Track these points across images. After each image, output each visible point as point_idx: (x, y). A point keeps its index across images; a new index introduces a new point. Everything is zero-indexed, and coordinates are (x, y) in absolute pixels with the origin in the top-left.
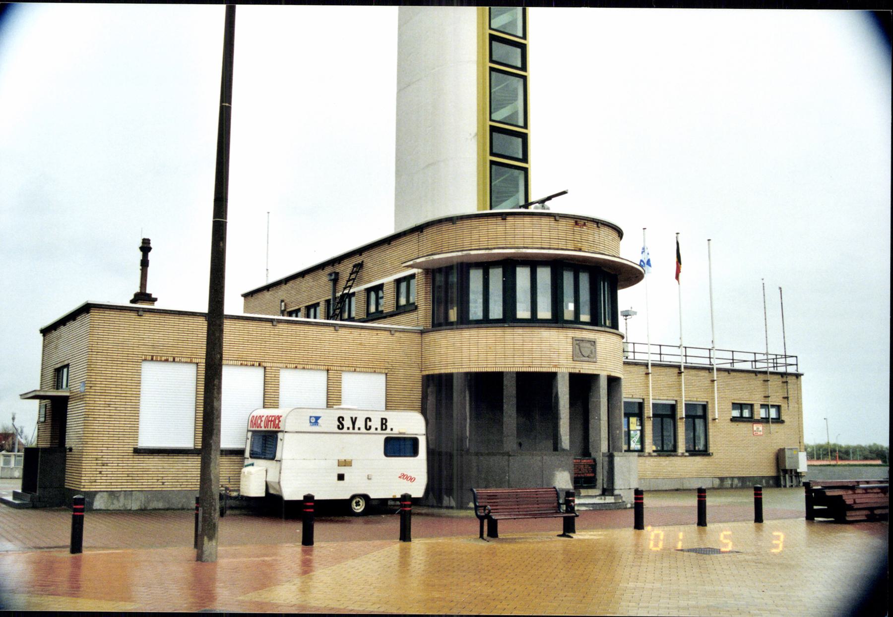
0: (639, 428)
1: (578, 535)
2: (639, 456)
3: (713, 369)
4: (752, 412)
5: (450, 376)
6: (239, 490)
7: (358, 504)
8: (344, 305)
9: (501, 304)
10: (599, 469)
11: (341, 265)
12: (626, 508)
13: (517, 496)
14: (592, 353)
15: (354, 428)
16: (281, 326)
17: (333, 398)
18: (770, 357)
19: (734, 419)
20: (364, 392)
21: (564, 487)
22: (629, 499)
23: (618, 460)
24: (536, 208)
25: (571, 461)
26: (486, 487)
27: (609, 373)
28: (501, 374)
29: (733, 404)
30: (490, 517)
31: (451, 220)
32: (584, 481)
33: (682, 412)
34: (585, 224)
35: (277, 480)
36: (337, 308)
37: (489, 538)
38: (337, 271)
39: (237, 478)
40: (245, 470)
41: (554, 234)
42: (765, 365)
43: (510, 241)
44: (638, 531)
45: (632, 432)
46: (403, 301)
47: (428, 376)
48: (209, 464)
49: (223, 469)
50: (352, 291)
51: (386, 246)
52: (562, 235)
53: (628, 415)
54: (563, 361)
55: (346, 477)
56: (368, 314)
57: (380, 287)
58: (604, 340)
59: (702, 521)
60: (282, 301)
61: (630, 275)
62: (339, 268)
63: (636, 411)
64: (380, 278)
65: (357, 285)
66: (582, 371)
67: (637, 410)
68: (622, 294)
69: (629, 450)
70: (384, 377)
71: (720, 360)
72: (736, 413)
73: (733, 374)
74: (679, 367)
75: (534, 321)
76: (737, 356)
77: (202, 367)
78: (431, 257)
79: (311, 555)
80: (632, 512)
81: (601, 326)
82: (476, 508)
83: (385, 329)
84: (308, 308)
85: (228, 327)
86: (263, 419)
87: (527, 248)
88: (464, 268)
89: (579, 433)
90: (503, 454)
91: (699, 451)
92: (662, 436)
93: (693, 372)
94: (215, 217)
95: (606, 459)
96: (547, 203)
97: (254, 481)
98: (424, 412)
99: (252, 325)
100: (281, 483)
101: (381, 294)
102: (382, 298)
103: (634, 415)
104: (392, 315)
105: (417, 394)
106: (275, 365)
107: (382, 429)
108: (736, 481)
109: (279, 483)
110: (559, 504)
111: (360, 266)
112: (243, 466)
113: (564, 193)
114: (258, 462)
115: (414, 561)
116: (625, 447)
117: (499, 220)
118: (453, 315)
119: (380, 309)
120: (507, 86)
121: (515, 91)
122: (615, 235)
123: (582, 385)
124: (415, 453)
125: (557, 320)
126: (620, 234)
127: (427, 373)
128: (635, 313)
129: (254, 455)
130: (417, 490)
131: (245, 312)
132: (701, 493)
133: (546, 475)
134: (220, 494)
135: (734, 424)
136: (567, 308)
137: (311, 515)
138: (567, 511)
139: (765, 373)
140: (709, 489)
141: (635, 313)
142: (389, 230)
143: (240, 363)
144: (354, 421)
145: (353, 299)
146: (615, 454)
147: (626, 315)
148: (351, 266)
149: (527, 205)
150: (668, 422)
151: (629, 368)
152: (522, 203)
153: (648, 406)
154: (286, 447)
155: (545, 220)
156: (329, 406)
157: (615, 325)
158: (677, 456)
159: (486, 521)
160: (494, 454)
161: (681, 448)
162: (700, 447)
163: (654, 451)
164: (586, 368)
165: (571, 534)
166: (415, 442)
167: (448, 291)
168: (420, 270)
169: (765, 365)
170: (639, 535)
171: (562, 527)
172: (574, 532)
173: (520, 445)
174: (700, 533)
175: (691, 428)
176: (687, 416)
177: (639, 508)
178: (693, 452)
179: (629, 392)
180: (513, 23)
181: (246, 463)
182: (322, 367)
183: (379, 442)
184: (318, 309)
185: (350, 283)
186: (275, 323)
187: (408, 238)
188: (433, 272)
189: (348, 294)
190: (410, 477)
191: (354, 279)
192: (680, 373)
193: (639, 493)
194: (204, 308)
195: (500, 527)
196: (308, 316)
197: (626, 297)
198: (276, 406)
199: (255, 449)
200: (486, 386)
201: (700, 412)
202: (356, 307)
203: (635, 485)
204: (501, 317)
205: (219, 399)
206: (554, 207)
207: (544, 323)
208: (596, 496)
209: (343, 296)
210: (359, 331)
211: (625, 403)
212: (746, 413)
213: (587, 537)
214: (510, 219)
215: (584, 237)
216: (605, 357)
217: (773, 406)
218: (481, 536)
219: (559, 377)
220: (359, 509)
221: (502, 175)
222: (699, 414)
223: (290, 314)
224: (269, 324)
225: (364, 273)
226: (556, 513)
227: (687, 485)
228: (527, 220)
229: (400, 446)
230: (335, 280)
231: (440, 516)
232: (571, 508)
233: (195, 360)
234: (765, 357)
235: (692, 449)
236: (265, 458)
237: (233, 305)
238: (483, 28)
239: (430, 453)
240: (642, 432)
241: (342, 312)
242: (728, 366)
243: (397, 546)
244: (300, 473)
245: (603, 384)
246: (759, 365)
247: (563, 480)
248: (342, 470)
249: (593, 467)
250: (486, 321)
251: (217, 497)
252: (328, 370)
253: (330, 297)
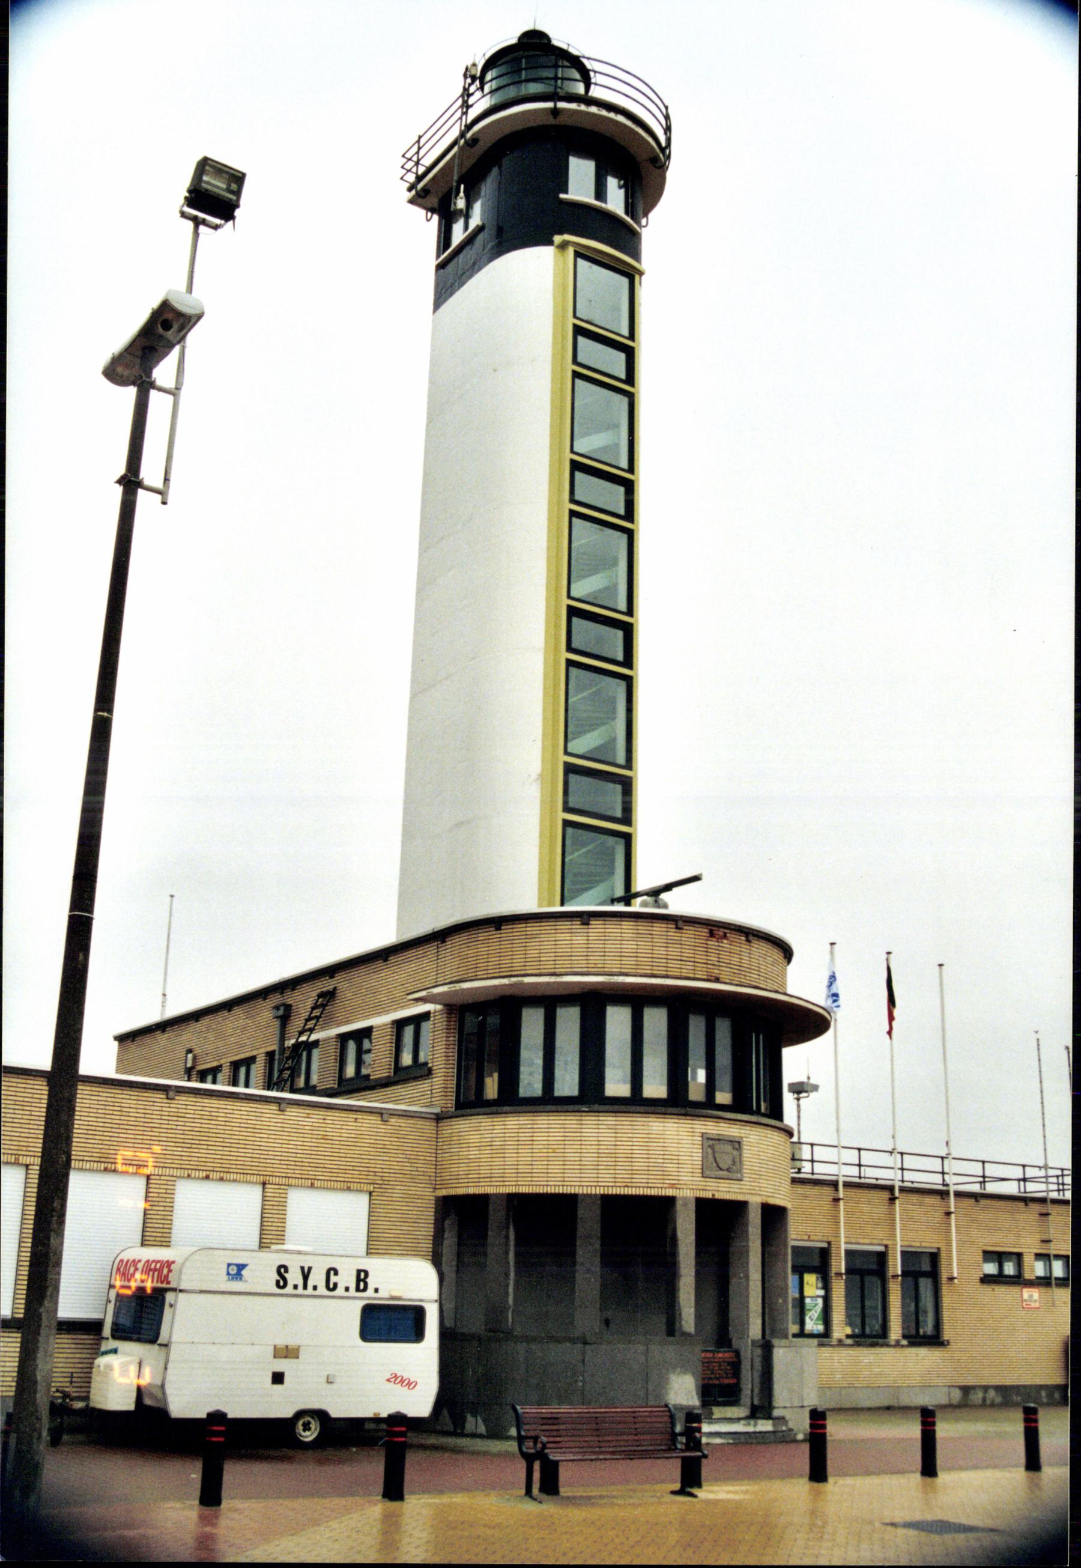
0: (822, 1292)
1: (709, 1492)
2: (821, 1345)
3: (947, 1193)
4: (1019, 1265)
5: (483, 1200)
6: (86, 1398)
7: (307, 1427)
8: (299, 1063)
9: (578, 1021)
10: (746, 1367)
11: (296, 993)
12: (795, 1441)
13: (596, 1419)
14: (734, 1163)
15: (305, 1287)
16: (182, 1099)
17: (271, 1232)
18: (1051, 1172)
19: (986, 1279)
20: (329, 1223)
21: (684, 1402)
22: (801, 1425)
23: (781, 1354)
24: (644, 904)
25: (696, 1353)
26: (540, 1403)
27: (765, 1200)
28: (571, 1200)
29: (985, 1252)
30: (546, 1455)
31: (498, 923)
32: (718, 1392)
33: (895, 1265)
34: (725, 936)
35: (159, 1383)
36: (287, 1069)
37: (544, 1497)
38: (290, 1001)
39: (85, 1376)
40: (102, 1361)
41: (674, 951)
42: (1043, 1187)
43: (595, 959)
44: (815, 1485)
45: (808, 1301)
46: (407, 1059)
47: (446, 1199)
48: (35, 1350)
49: (59, 1358)
50: (314, 1037)
51: (380, 964)
52: (688, 953)
53: (800, 1270)
54: (686, 1178)
55: (286, 1379)
56: (341, 1079)
57: (367, 1032)
58: (756, 1141)
59: (929, 1469)
60: (190, 1051)
61: (808, 1023)
62: (293, 998)
63: (816, 1261)
64: (367, 1017)
65: (323, 1029)
66: (718, 1196)
67: (817, 1261)
68: (789, 1054)
69: (802, 1334)
70: (365, 1198)
71: (962, 1177)
72: (991, 1268)
73: (983, 1202)
74: (890, 1189)
75: (636, 1103)
76: (991, 1170)
77: (35, 1172)
78: (458, 986)
79: (214, 1525)
80: (806, 1448)
81: (752, 1113)
82: (520, 1439)
83: (371, 1111)
84: (236, 1065)
85: (84, 1097)
86: (140, 1266)
87: (627, 975)
89: (712, 1293)
90: (573, 1341)
91: (925, 1336)
92: (863, 1307)
93: (914, 1198)
94: (73, 908)
95: (759, 1351)
96: (664, 896)
97: (120, 1378)
98: (437, 1261)
99: (128, 1099)
100: (167, 1386)
101: (366, 1044)
102: (369, 1051)
103: (811, 1270)
104: (385, 1084)
105: (426, 1229)
106: (167, 1172)
107: (358, 1289)
108: (992, 1393)
109: (163, 1386)
110: (674, 1435)
111: (329, 996)
112: (97, 1352)
113: (696, 878)
114: (125, 1346)
115: (406, 1540)
116: (794, 1329)
117: (576, 925)
118: (492, 1087)
119: (364, 1071)
120: (599, 690)
121: (613, 701)
122: (777, 955)
123: (720, 1219)
124: (418, 1335)
125: (677, 1102)
126: (786, 952)
127: (443, 1193)
128: (815, 1088)
129: (120, 1333)
130: (420, 1402)
131: (117, 1071)
132: (928, 1417)
133: (652, 1381)
134: (52, 1404)
135: (987, 1289)
136: (694, 1077)
137: (220, 1446)
138: (688, 1448)
139: (1043, 1201)
140: (943, 1407)
141: (815, 1088)
142: (388, 937)
143: (103, 1166)
144: (306, 1275)
145: (315, 1053)
146: (776, 1342)
147: (799, 1089)
148: (314, 994)
149: (627, 899)
150: (873, 1282)
151: (800, 1189)
152: (620, 892)
153: (839, 1255)
154: (182, 1320)
155: (659, 928)
156: (262, 1245)
157: (776, 1111)
158: (888, 1345)
159: (537, 1466)
160: (558, 1341)
161: (895, 1331)
162: (928, 1328)
163: (848, 1336)
164: (725, 1190)
165: (695, 1491)
166: (418, 1314)
168: (439, 1007)
169: (1043, 1187)
170: (817, 1494)
171: (679, 1479)
172: (700, 1486)
173: (607, 1322)
174: (926, 1490)
175: (912, 1295)
176: (905, 1274)
177: (817, 1442)
178: (916, 1338)
179: (800, 1232)
180: (611, 589)
181: (103, 1348)
182: (254, 1179)
183: (351, 1312)
184: (253, 1067)
185: (310, 1024)
186: (171, 1094)
187: (420, 951)
188: (459, 1011)
189: (306, 1043)
190: (405, 1379)
191: (318, 1018)
192: (893, 1199)
193: (818, 1417)
194: (45, 1062)
195: (565, 1474)
196: (235, 1083)
197: (797, 1061)
198: (166, 1244)
199: (121, 1321)
200: (544, 1221)
201: (926, 1267)
202: (320, 1068)
203: (812, 1399)
204: (575, 1092)
205: (60, 1233)
206: (677, 903)
207: (654, 1107)
208: (739, 1419)
209: (297, 1046)
210: (323, 1112)
211: (793, 1247)
212: (1009, 1269)
213: (722, 1496)
214: (595, 923)
215: (725, 957)
216: (759, 1173)
217: (1058, 1257)
218: (529, 1492)
219: (679, 1204)
220: (309, 1436)
221: (584, 845)
222: (925, 1268)
223: (202, 1076)
224: (160, 1096)
225: (337, 1008)
226: (669, 1450)
227: (906, 1400)
228: (627, 926)
229: (388, 1322)
230: (285, 1016)
231: (457, 1451)
232: (694, 1443)
233: (22, 1160)
234: (1042, 1173)
235: (913, 1332)
236: (139, 1340)
237: (98, 1056)
238: (556, 649)
239: (445, 1335)
240: (827, 1299)
241: (294, 1072)
242: (976, 1188)
243: (377, 1508)
244: (205, 1370)
245: (754, 1219)
246: (1031, 1187)
247: (682, 1390)
248: (280, 1365)
249: (735, 1366)
250: (548, 1101)
251: (44, 1413)
252: (264, 1184)
253: (275, 1047)
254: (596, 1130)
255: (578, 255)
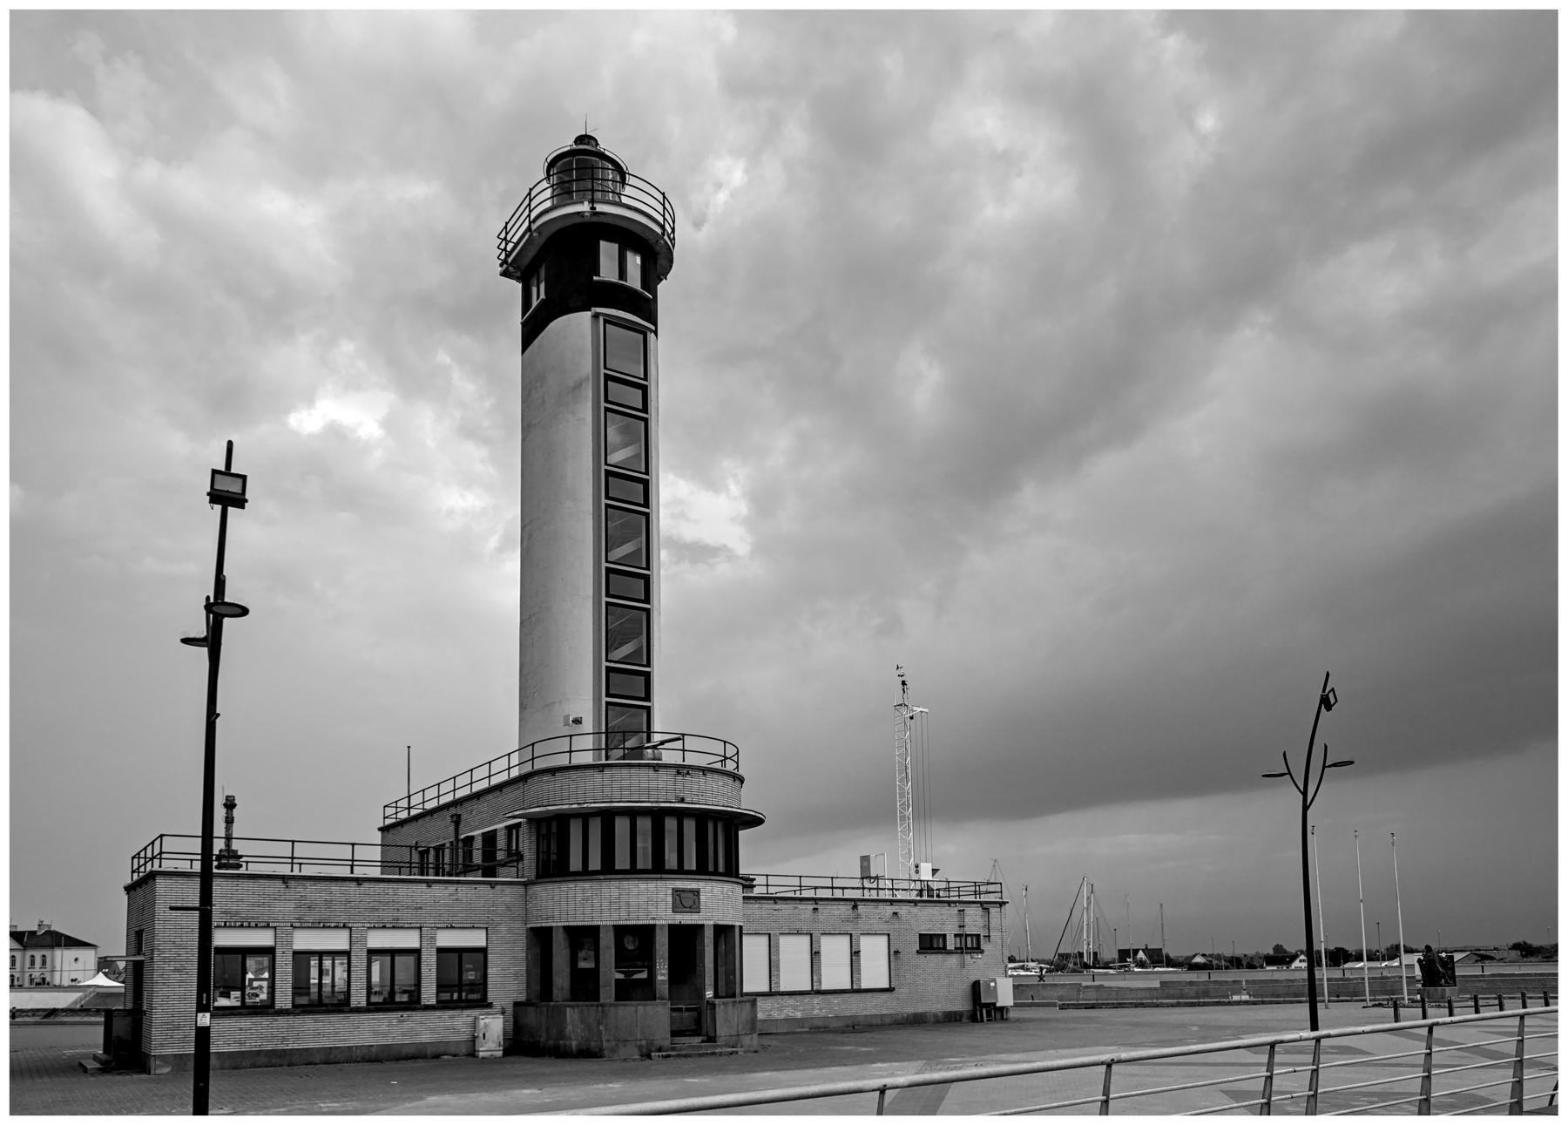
88: (563, 819)
123: (685, 938)
125: (658, 868)
167: (558, 843)
188: (536, 822)
194: (216, 882)
230: (457, 820)
245: (709, 935)
250: (585, 873)
254: (611, 890)
255: (605, 321)
